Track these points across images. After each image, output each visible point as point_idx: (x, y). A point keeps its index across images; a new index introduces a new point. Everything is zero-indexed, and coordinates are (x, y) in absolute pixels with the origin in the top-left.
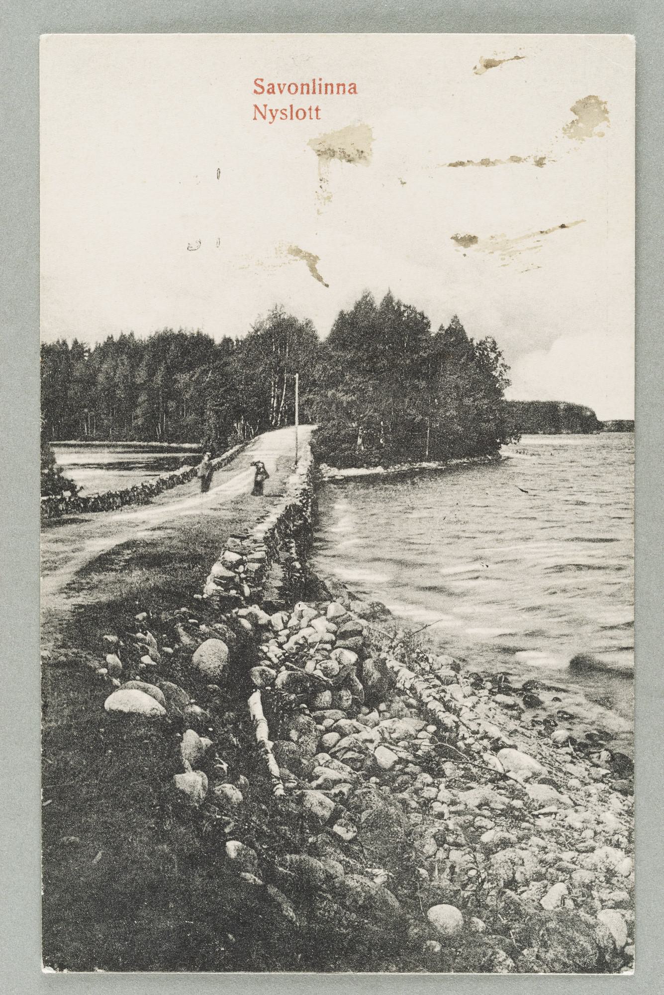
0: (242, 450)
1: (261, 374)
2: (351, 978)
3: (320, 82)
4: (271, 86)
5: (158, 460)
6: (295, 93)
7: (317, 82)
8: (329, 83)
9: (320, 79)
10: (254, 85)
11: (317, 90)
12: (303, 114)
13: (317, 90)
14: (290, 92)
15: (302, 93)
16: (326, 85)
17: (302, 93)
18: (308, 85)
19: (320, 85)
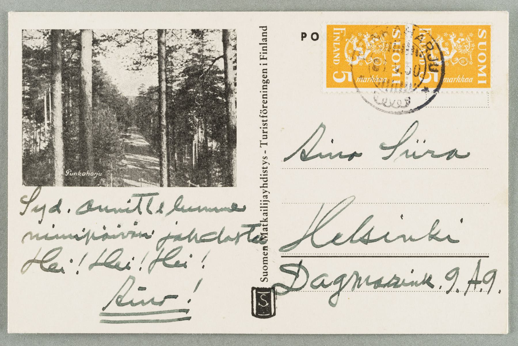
0: (182, 200)
1: (117, 165)
2: (507, 94)
3: (262, 204)
4: (264, 230)
5: (275, 298)
6: (264, 269)
7: (263, 205)
8: (262, 71)
9: (261, 175)
10: (264, 281)
11: (265, 206)
12: (265, 267)
13: (265, 206)
14: (263, 267)
15: (267, 264)
16: (263, 50)
17: (267, 264)
18: (263, 47)
19: (264, 204)
